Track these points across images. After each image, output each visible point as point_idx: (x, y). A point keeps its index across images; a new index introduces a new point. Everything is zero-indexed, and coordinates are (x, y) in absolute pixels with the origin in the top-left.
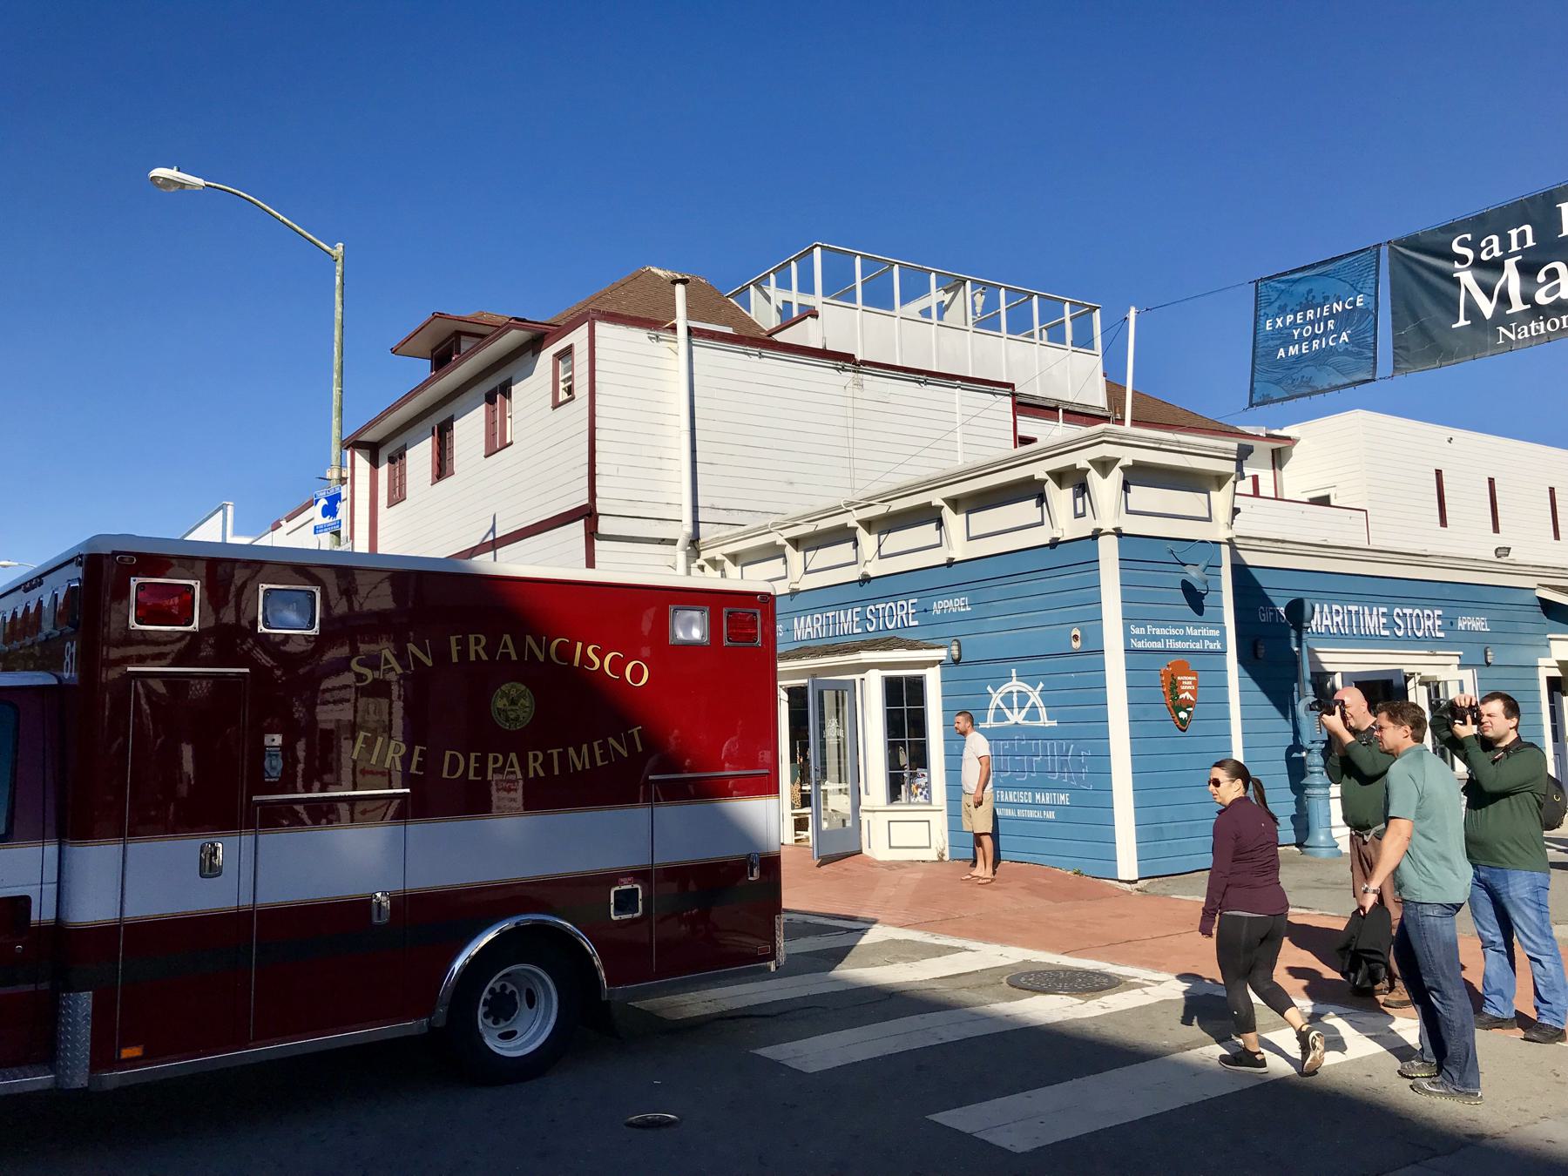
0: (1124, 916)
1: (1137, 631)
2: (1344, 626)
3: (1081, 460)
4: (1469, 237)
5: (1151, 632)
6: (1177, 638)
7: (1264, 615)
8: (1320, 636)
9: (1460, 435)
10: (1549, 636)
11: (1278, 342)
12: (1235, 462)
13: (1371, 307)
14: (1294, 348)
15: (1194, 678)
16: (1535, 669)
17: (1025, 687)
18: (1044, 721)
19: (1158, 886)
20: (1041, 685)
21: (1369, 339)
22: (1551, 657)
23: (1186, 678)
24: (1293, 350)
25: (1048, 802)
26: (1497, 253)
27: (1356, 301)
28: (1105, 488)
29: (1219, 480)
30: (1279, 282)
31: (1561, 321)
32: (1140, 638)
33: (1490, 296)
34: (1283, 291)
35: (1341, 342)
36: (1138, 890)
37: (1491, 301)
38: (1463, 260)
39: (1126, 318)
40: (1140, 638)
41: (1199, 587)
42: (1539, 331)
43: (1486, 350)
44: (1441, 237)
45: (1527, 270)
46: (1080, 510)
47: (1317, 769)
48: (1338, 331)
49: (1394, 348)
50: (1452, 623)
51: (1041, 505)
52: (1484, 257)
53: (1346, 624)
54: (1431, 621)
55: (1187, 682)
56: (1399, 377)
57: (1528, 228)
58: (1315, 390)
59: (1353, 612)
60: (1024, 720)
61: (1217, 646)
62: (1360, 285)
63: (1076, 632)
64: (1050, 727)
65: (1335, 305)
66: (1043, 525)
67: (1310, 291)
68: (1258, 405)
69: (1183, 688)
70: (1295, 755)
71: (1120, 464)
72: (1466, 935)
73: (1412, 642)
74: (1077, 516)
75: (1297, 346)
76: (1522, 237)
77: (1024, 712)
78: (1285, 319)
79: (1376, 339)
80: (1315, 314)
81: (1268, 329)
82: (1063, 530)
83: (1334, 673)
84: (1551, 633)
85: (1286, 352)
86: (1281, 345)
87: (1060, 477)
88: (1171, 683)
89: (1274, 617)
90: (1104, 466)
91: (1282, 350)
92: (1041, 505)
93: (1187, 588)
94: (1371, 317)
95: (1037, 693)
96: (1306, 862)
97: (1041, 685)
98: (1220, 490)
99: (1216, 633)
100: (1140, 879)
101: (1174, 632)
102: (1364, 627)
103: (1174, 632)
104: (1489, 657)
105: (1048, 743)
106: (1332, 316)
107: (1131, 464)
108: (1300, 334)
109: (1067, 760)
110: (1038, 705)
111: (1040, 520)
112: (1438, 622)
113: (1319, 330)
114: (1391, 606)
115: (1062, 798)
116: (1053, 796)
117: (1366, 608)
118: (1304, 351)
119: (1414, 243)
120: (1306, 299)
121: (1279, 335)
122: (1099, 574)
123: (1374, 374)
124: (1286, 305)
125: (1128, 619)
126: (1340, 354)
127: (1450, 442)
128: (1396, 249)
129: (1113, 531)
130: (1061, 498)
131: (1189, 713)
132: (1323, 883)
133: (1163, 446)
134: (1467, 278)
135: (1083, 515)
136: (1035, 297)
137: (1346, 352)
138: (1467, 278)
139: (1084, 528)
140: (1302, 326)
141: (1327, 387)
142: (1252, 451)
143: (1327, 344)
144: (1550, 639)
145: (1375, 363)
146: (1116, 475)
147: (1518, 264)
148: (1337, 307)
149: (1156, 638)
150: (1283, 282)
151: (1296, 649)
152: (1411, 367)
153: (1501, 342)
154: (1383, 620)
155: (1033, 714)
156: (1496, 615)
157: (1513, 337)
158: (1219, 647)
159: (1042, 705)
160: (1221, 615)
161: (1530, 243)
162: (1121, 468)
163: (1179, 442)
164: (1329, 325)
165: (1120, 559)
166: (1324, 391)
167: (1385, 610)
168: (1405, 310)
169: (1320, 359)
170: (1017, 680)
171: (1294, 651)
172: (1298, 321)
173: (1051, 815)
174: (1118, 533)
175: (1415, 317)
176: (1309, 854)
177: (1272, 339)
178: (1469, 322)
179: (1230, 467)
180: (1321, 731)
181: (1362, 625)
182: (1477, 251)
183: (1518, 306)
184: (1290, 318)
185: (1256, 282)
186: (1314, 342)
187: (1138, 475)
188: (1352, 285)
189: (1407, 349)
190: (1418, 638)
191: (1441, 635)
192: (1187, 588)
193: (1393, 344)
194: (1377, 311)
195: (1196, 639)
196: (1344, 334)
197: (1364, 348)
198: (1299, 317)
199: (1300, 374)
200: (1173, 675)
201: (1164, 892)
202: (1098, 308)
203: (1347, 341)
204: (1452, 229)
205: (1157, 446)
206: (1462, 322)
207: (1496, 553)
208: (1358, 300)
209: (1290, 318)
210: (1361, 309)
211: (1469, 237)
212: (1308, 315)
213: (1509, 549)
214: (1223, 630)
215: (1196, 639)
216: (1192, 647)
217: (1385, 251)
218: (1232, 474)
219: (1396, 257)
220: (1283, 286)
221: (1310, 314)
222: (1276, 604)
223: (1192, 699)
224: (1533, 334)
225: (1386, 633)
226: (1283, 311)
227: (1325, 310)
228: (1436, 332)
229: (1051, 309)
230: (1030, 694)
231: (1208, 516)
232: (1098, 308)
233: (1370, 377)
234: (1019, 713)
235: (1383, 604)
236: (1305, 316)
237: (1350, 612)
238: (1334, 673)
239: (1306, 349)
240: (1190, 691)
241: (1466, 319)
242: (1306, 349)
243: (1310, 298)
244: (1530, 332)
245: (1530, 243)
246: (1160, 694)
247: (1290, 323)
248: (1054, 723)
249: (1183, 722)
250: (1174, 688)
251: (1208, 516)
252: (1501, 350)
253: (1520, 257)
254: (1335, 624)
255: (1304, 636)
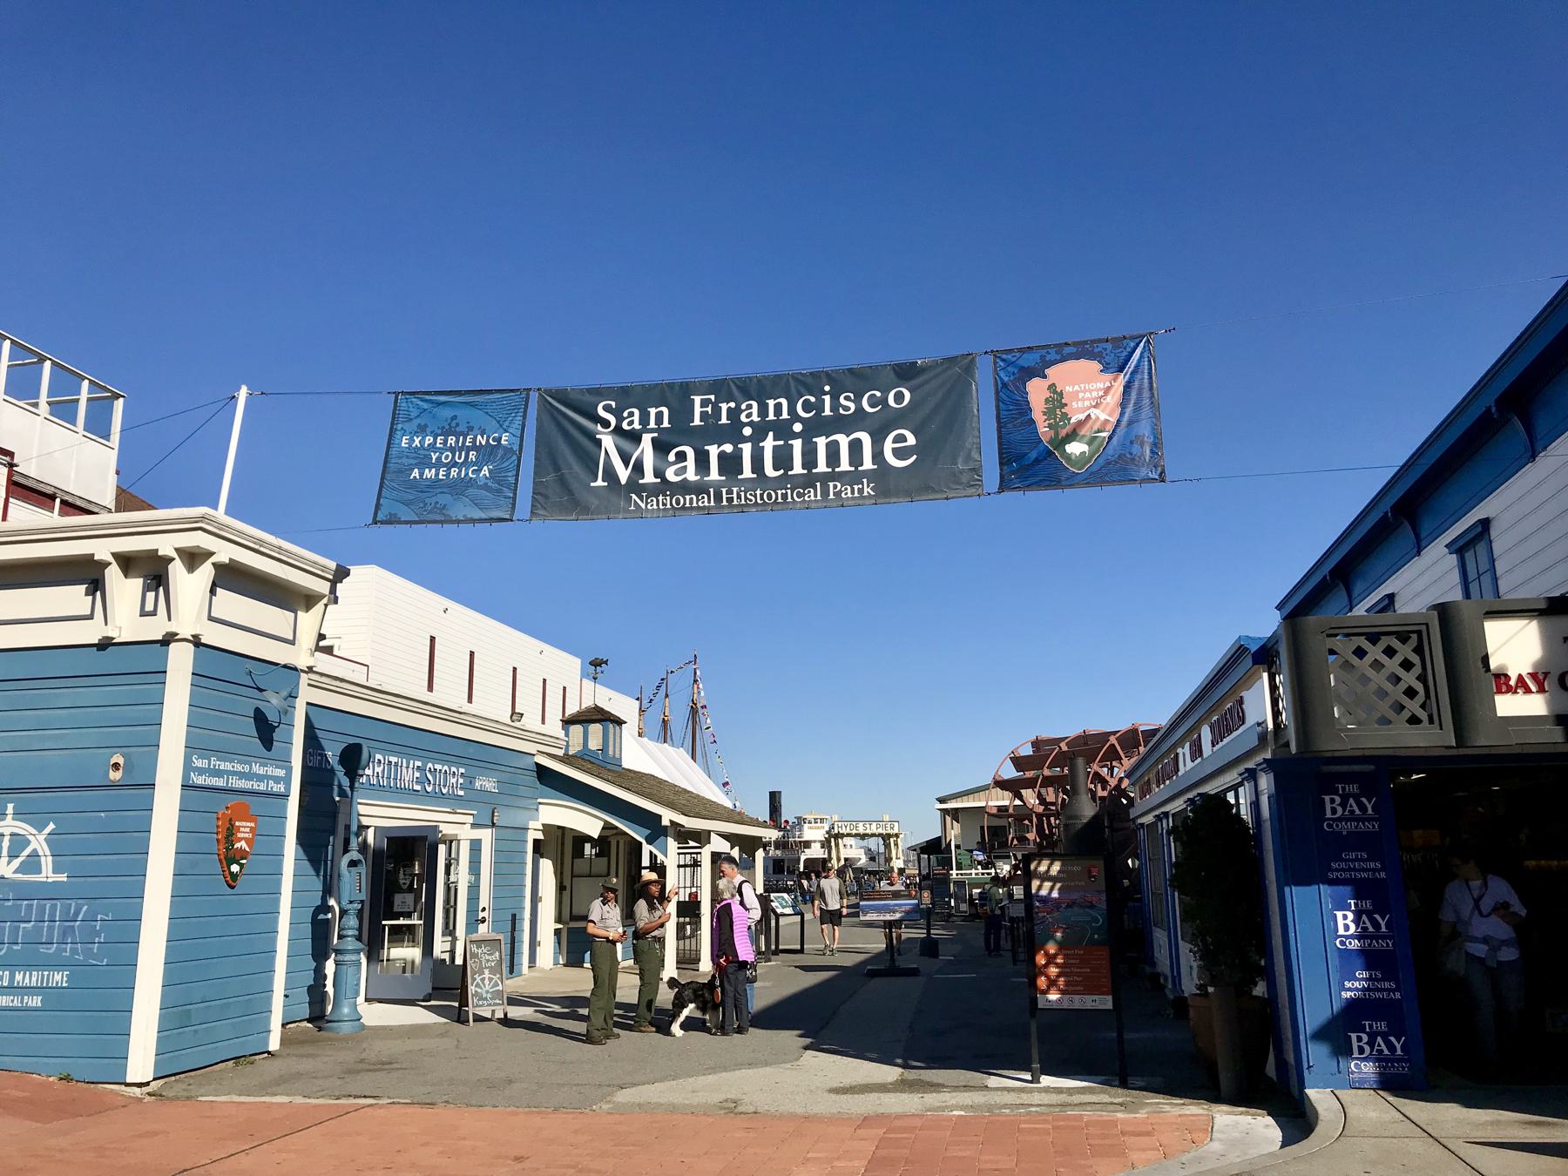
0: (155, 1134)
1: (198, 763)
2: (383, 777)
3: (166, 545)
4: (613, 404)
5: (215, 766)
6: (242, 775)
7: (312, 758)
8: (382, 788)
9: (454, 607)
10: (539, 800)
11: (414, 462)
12: (329, 584)
13: (516, 448)
14: (430, 471)
15: (252, 825)
16: (524, 831)
17: (23, 828)
18: (48, 872)
19: (177, 1087)
20: (51, 826)
21: (509, 479)
22: (538, 820)
23: (244, 824)
24: (429, 474)
25: (34, 984)
26: (637, 426)
27: (501, 438)
28: (189, 586)
29: (308, 600)
30: (422, 400)
31: (685, 499)
32: (201, 771)
33: (626, 463)
34: (425, 410)
35: (481, 475)
36: (149, 1094)
37: (627, 468)
38: (606, 424)
39: (234, 397)
40: (201, 771)
41: (272, 717)
42: (666, 505)
43: (619, 513)
44: (589, 398)
45: (661, 447)
46: (149, 607)
47: (350, 933)
48: (479, 464)
49: (534, 493)
50: (471, 782)
51: (93, 594)
52: (625, 426)
53: (386, 776)
54: (453, 778)
55: (244, 828)
56: (535, 522)
57: (665, 410)
58: (449, 519)
59: (393, 763)
60: (14, 873)
61: (280, 788)
62: (507, 423)
63: (118, 758)
64: (54, 882)
65: (479, 437)
66: (92, 619)
67: (455, 417)
68: (382, 522)
69: (240, 835)
70: (321, 917)
71: (213, 559)
72: (550, 1110)
73: (438, 798)
74: (143, 614)
75: (434, 470)
76: (659, 416)
77: (16, 863)
78: (424, 439)
79: (517, 480)
80: (457, 441)
81: (403, 445)
82: (120, 628)
83: (368, 827)
84: (541, 798)
85: (421, 474)
86: (416, 465)
87: (128, 563)
88: (228, 829)
89: (321, 761)
90: (193, 558)
91: (416, 470)
92: (93, 594)
93: (260, 718)
94: (515, 457)
95: (42, 838)
96: (330, 1039)
97: (51, 826)
98: (307, 611)
99: (281, 773)
100: (154, 1079)
101: (239, 768)
102: (400, 780)
103: (239, 768)
104: (495, 818)
105: (48, 904)
106: (474, 447)
107: (227, 561)
108: (439, 459)
109: (73, 926)
110: (41, 853)
111: (89, 613)
112: (461, 781)
113: (460, 458)
114: (426, 759)
115: (58, 977)
116: (43, 976)
117: (404, 760)
118: (441, 477)
119: (562, 396)
120: (449, 425)
121: (415, 455)
122: (164, 688)
123: (512, 515)
124: (426, 426)
125: (191, 748)
126: (480, 487)
127: (445, 612)
128: (546, 399)
129: (191, 638)
130: (124, 590)
131: (242, 866)
132: (369, 1064)
133: (262, 549)
134: (608, 442)
135: (154, 613)
136: (48, 364)
137: (485, 487)
138: (608, 442)
139: (154, 629)
140: (441, 451)
141: (462, 518)
142: (348, 575)
143: (467, 474)
144: (540, 803)
145: (514, 505)
146: (206, 572)
147: (653, 440)
148: (481, 440)
149: (218, 773)
150: (426, 401)
151: (337, 799)
152: (549, 515)
153: (632, 508)
154: (417, 774)
155: (33, 864)
156: (505, 777)
157: (643, 506)
158: (282, 790)
159: (48, 853)
160: (289, 752)
161: (666, 424)
162: (213, 564)
163: (280, 548)
164: (470, 456)
165: (193, 674)
166: (458, 522)
167: (418, 763)
168: (547, 458)
169: (459, 488)
170: (13, 819)
171: (334, 800)
172: (438, 445)
173: (35, 1001)
174: (196, 642)
175: (557, 468)
176: (330, 1029)
177: (407, 457)
178: (606, 484)
179: (323, 587)
180: (360, 890)
181: (399, 778)
182: (620, 419)
183: (649, 478)
184: (429, 440)
185: (397, 394)
186: (453, 470)
187: (232, 577)
188: (498, 422)
189: (546, 497)
190: (443, 794)
191: (461, 793)
192: (260, 718)
193: (534, 489)
194: (520, 453)
195: (260, 778)
196: (485, 468)
197: (503, 486)
198: (439, 441)
199: (433, 500)
200: (231, 819)
201: (186, 1094)
202: (123, 397)
203: (488, 475)
204: (600, 393)
205: (257, 547)
206: (600, 483)
207: (511, 717)
208: (503, 438)
209: (429, 440)
210: (505, 447)
211: (613, 404)
212: (449, 442)
213: (522, 715)
214: (289, 770)
215: (260, 778)
216: (255, 787)
217: (534, 396)
218: (325, 596)
219: (543, 403)
220: (425, 406)
221: (451, 440)
222: (325, 748)
223: (247, 849)
224: (661, 507)
225: (417, 787)
226: (422, 430)
227: (468, 440)
228: (575, 486)
229: (66, 380)
230: (30, 837)
231: (291, 638)
232: (123, 397)
233: (508, 517)
234: (9, 863)
235: (418, 757)
236: (445, 442)
237: (390, 762)
238: (368, 827)
239: (443, 475)
240: (246, 840)
241: (603, 481)
242: (443, 475)
243: (453, 424)
244: (658, 505)
245: (666, 424)
246: (212, 844)
247: (429, 445)
248: (63, 878)
249: (234, 876)
250: (230, 834)
251: (291, 638)
252: (632, 515)
253: (656, 435)
254: (375, 774)
255: (357, 785)
